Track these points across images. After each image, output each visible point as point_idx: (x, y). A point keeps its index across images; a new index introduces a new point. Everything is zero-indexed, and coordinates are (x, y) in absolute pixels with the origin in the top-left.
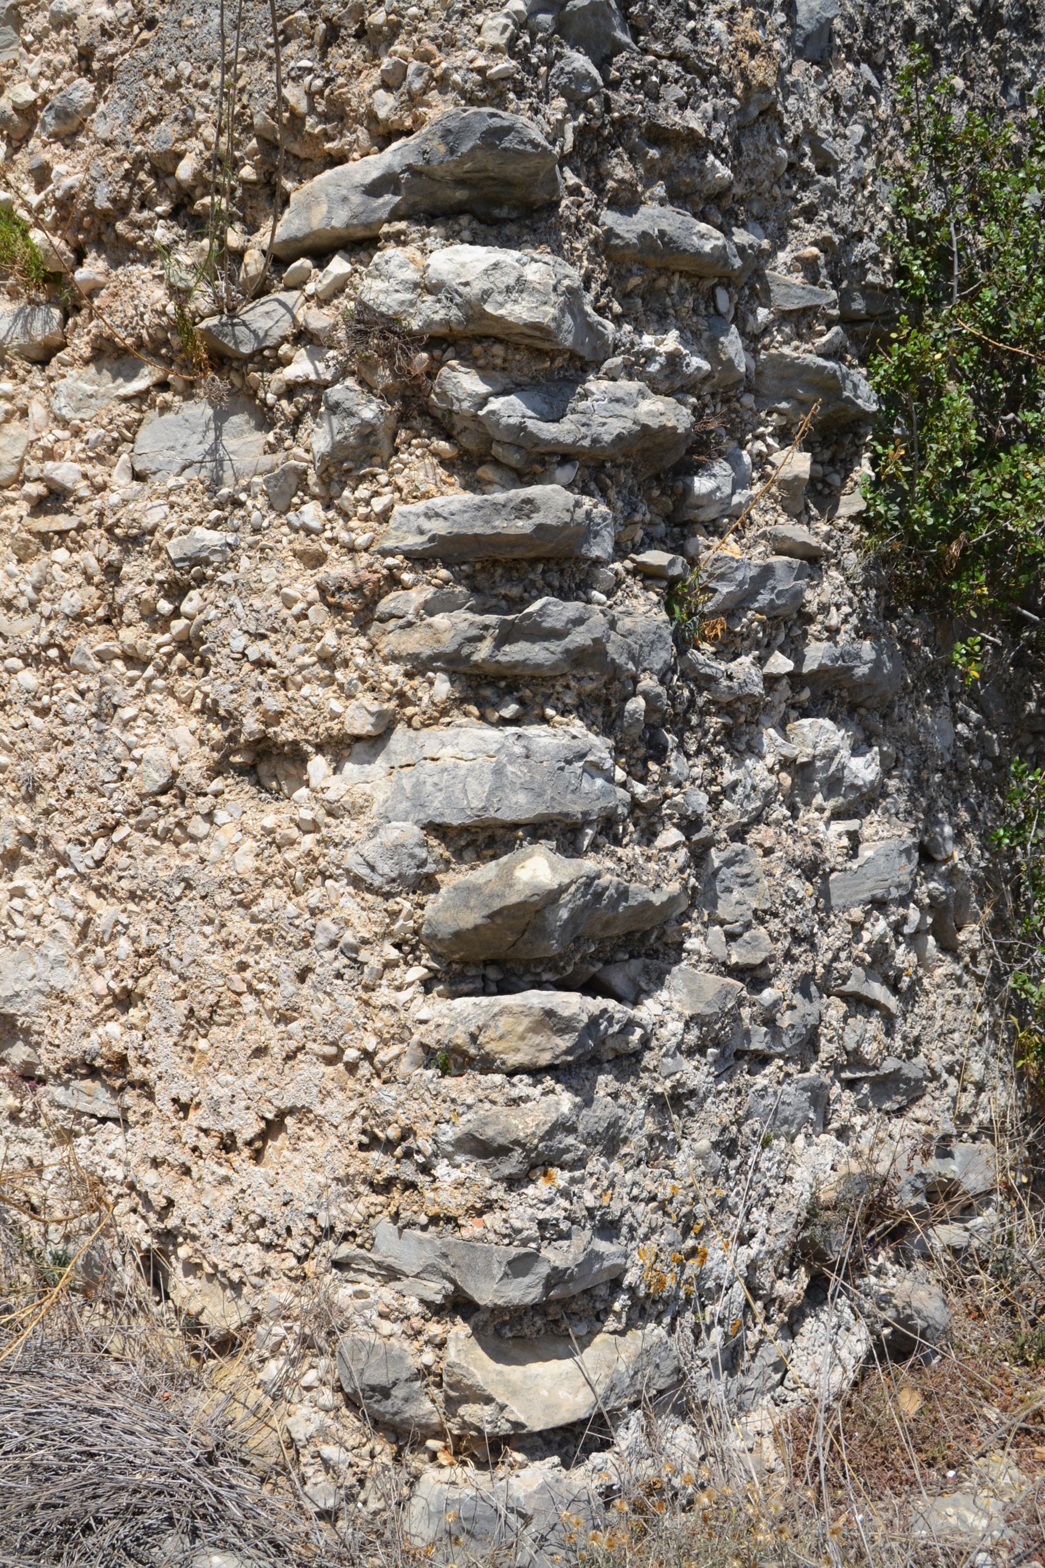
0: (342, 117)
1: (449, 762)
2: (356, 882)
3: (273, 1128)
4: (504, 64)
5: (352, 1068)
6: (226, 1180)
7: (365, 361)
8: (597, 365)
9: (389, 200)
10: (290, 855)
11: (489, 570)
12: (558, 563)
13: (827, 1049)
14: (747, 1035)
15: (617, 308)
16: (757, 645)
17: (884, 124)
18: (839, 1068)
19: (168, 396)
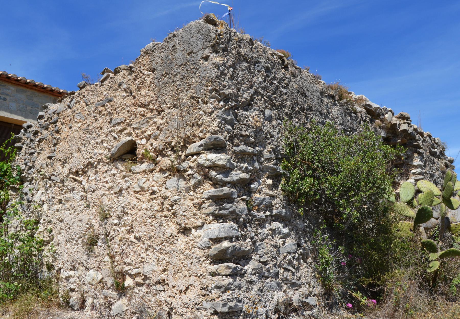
0: (195, 136)
1: (212, 229)
2: (199, 248)
3: (187, 288)
4: (217, 129)
5: (199, 277)
6: (180, 298)
7: (199, 171)
8: (234, 169)
9: (202, 148)
10: (189, 245)
11: (217, 200)
12: (228, 198)
13: (280, 277)
14: (264, 273)
15: (237, 161)
16: (264, 210)
17: (283, 129)
18: (283, 281)
19: (171, 177)
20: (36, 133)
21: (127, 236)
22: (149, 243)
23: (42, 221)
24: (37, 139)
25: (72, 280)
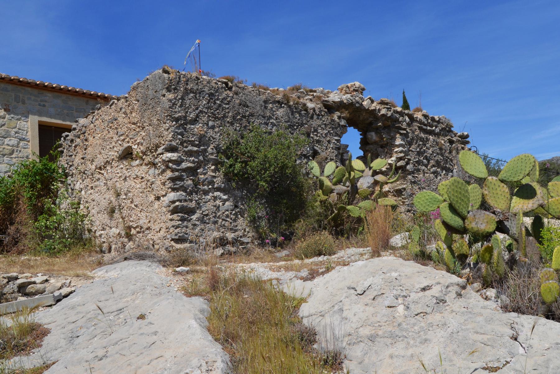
3: (160, 230)
11: (173, 180)
20: (72, 141)
21: (131, 205)
22: (141, 207)
23: (82, 202)
24: (73, 145)
25: (103, 236)
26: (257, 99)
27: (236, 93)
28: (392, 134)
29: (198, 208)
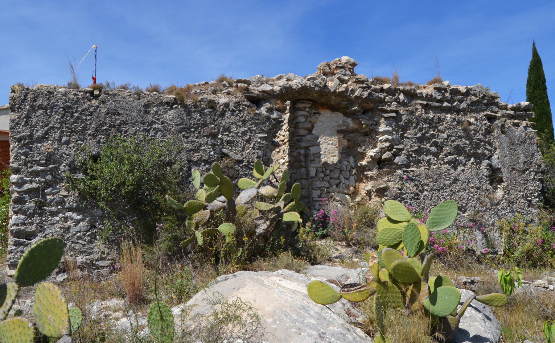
26: (134, 105)
27: (104, 102)
28: (376, 119)
29: (40, 231)
